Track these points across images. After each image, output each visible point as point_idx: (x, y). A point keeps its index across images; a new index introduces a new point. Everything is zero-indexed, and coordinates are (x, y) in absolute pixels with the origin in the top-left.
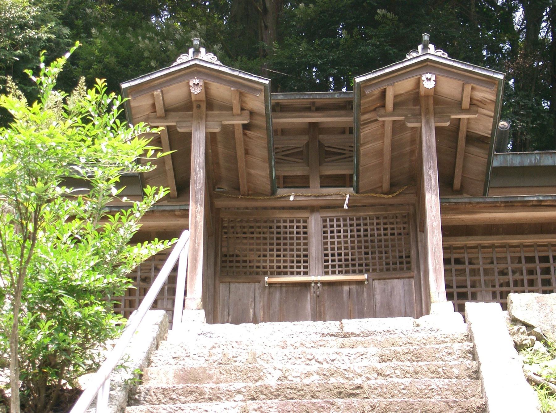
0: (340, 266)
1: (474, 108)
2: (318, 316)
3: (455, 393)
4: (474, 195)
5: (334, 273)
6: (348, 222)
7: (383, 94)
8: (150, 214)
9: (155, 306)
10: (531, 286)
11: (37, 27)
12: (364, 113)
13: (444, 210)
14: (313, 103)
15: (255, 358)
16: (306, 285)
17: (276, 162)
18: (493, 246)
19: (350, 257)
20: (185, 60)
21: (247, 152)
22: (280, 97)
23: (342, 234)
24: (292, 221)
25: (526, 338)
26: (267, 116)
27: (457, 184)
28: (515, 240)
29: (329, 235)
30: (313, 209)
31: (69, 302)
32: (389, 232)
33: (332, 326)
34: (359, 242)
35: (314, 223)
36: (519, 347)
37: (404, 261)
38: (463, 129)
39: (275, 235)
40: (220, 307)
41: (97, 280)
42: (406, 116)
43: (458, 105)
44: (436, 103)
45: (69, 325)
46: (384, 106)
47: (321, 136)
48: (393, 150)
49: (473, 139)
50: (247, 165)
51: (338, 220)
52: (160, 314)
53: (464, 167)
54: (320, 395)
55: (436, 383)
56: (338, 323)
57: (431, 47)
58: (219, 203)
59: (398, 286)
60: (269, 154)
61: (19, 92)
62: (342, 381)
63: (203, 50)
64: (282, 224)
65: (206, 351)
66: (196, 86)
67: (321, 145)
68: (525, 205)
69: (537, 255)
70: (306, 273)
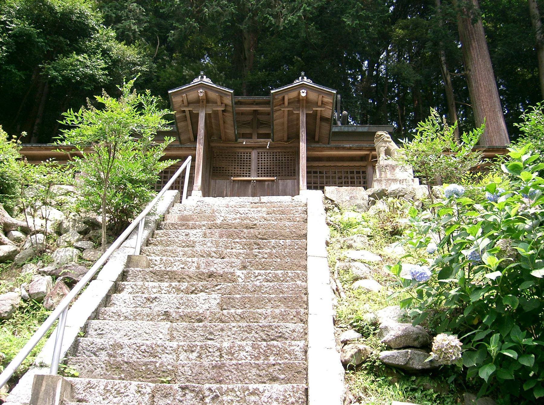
0: (264, 173)
1: (324, 105)
2: (254, 195)
3: (296, 228)
4: (324, 144)
5: (261, 176)
6: (269, 154)
7: (284, 98)
8: (166, 150)
9: (171, 188)
10: (334, 184)
11: (141, 65)
12: (275, 106)
13: (308, 150)
14: (255, 101)
15: (214, 211)
16: (249, 181)
17: (237, 127)
18: (330, 166)
19: (272, 169)
20: (197, 81)
21: (224, 123)
22: (240, 98)
23: (266, 159)
24: (244, 153)
25: (331, 206)
26: (232, 106)
27: (317, 138)
28: (340, 164)
29: (260, 159)
30: (253, 148)
31: (129, 185)
32: (287, 159)
33: (256, 199)
34: (273, 163)
35: (254, 154)
36: (327, 210)
37: (292, 172)
38: (319, 114)
39: (240, 159)
40: (211, 191)
41: (143, 177)
42: (293, 108)
43: (316, 105)
44: (307, 102)
45: (130, 196)
46: (284, 103)
47: (258, 116)
48: (288, 122)
49: (323, 119)
50: (224, 127)
51: (264, 153)
52: (175, 192)
53: (320, 131)
54: (238, 228)
55: (287, 224)
56: (259, 198)
57: (305, 78)
58: (213, 144)
59: (289, 182)
60: (234, 123)
61: (107, 95)
62: (249, 221)
63: (205, 77)
64: (240, 154)
65: (193, 208)
66: (201, 93)
67: (258, 120)
68: (344, 149)
69: (349, 171)
70: (249, 176)
